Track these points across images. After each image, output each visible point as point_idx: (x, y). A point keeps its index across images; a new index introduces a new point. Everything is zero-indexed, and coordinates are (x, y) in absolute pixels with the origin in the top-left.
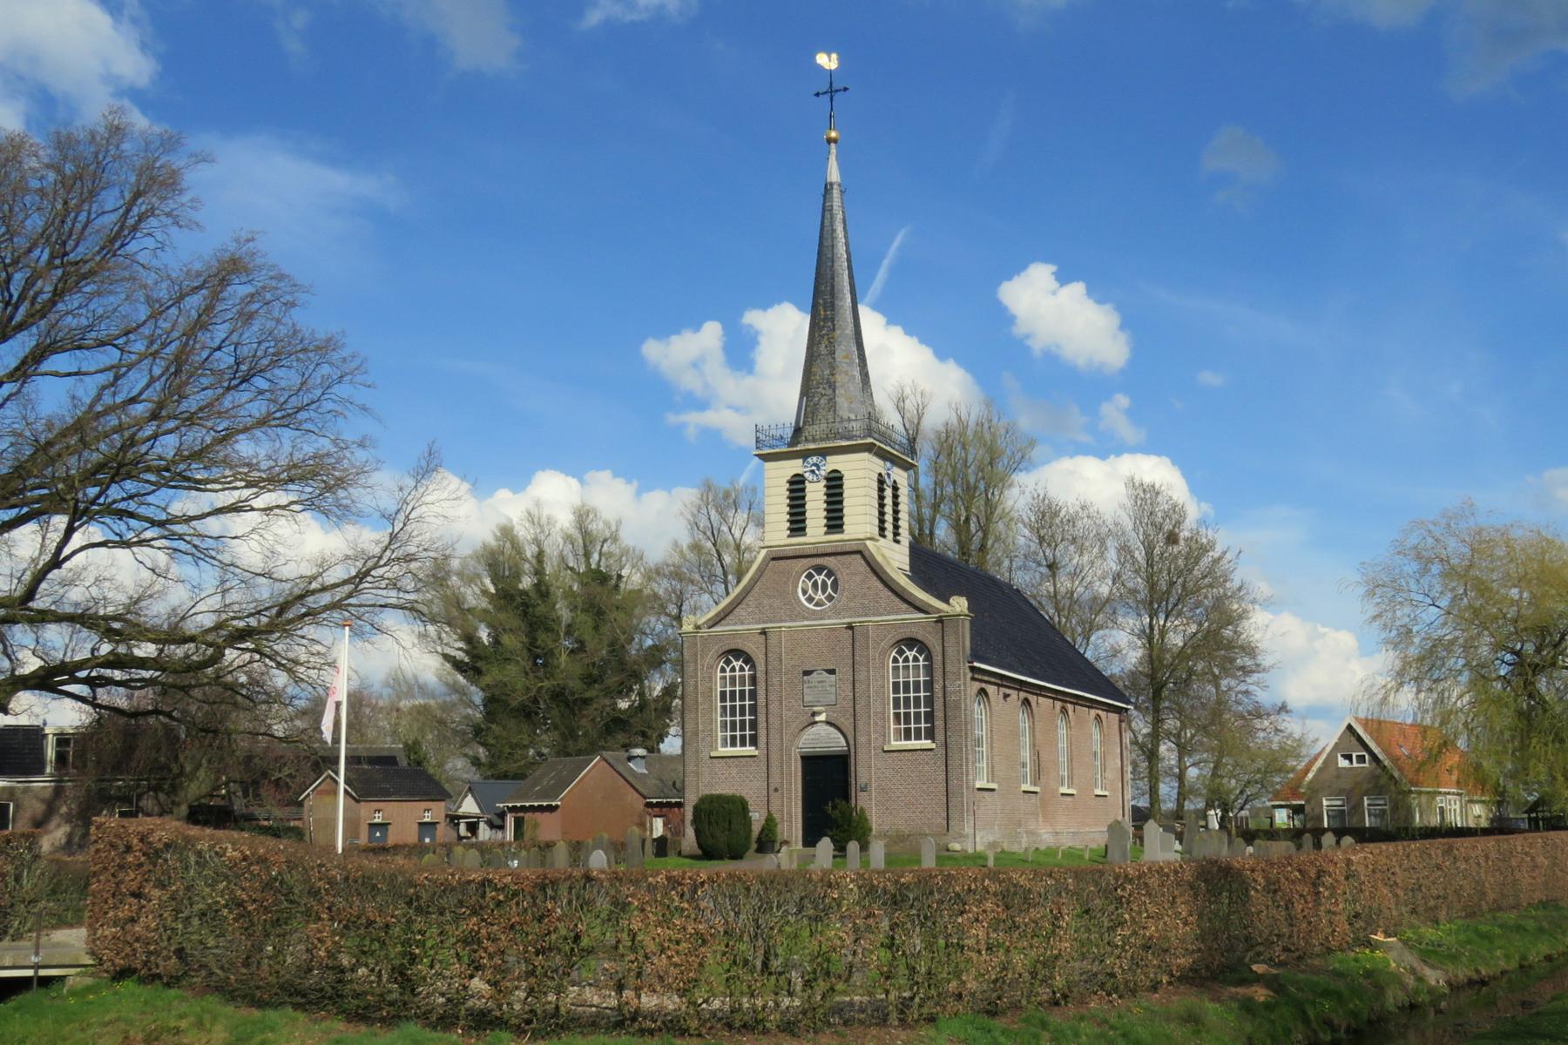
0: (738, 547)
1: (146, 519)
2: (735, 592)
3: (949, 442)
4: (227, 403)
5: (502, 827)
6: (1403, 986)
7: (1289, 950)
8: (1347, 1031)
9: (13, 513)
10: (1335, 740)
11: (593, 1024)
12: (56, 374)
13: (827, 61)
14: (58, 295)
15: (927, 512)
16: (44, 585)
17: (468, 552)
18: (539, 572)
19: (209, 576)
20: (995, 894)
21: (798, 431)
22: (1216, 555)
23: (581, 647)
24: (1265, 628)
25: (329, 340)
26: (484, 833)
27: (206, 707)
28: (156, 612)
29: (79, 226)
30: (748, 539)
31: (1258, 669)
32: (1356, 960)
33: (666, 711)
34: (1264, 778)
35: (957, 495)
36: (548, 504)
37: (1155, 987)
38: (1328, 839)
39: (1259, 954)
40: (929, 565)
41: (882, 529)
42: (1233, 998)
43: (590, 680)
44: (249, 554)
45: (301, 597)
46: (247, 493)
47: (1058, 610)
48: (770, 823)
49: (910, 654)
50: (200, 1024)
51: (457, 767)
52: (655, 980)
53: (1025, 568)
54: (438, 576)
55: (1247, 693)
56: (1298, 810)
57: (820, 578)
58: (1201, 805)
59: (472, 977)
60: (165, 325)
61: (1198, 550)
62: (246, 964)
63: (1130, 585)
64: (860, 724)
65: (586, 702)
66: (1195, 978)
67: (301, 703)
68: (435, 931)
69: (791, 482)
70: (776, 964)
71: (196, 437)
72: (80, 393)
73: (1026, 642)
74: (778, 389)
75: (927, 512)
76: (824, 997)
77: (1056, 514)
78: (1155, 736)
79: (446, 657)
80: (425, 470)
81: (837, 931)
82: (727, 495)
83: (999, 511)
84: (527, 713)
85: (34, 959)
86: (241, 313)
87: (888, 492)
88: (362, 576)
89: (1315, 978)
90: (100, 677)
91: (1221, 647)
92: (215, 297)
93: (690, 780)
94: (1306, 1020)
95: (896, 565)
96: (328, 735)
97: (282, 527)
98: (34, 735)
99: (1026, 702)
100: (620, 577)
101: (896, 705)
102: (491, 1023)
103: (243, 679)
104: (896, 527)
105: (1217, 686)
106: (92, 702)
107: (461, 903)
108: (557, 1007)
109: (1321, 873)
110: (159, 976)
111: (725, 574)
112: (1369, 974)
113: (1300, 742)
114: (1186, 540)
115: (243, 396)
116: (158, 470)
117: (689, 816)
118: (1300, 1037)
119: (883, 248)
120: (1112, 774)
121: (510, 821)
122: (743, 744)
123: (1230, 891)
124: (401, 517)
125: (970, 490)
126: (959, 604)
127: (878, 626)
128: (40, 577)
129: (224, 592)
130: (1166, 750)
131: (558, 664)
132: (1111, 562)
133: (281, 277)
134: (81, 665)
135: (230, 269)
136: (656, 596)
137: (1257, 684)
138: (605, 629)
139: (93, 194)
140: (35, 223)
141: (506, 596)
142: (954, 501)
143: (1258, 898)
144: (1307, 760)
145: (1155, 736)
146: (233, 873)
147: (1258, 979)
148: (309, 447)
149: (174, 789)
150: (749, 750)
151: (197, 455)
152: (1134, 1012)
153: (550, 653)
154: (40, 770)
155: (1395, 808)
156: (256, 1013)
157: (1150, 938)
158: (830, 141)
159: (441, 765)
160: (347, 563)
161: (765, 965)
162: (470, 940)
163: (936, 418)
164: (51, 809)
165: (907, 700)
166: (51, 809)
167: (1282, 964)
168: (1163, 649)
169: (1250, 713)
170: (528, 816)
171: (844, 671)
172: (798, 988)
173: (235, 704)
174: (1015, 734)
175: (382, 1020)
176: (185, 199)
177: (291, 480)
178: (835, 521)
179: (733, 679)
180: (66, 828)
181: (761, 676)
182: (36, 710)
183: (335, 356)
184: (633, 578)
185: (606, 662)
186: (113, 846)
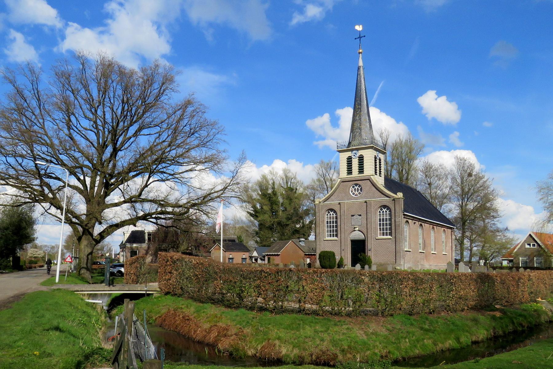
0: (331, 180)
1: (169, 174)
2: (330, 193)
3: (396, 147)
4: (188, 141)
5: (264, 260)
6: (547, 315)
7: (508, 302)
8: (528, 327)
9: (135, 173)
10: (525, 239)
11: (292, 311)
12: (144, 135)
13: (359, 28)
14: (144, 113)
15: (389, 168)
16: (143, 192)
17: (253, 181)
18: (273, 188)
19: (185, 189)
20: (412, 279)
21: (350, 143)
22: (485, 180)
23: (286, 209)
24: (502, 204)
25: (214, 122)
26: (259, 261)
27: (185, 225)
28: (172, 199)
29: (148, 93)
30: (334, 177)
31: (499, 216)
32: (531, 306)
33: (310, 228)
34: (499, 250)
35: (399, 163)
36: (276, 170)
37: (463, 310)
38: (522, 270)
39: (498, 303)
40: (390, 183)
41: (376, 172)
42: (488, 315)
43: (288, 219)
44: (196, 183)
45: (210, 194)
46: (194, 166)
47: (432, 198)
48: (341, 260)
49: (384, 210)
50: (187, 307)
51: (251, 243)
52: (310, 300)
53: (420, 184)
54: (246, 189)
55: (494, 224)
56: (511, 261)
57: (356, 188)
58: (478, 259)
59: (258, 297)
60: (171, 120)
61: (479, 178)
62: (198, 292)
63: (455, 190)
64: (369, 231)
65: (287, 225)
66: (475, 308)
67: (210, 225)
68: (248, 284)
69: (348, 159)
70: (345, 297)
71: (180, 151)
72: (151, 139)
73: (421, 207)
74: (344, 132)
75: (389, 168)
76: (359, 307)
77: (431, 168)
78: (463, 237)
79: (248, 212)
80: (242, 160)
81: (362, 288)
82: (328, 164)
83: (412, 167)
84: (271, 228)
85: (145, 289)
86: (191, 116)
87: (378, 161)
88: (225, 188)
89: (517, 311)
90: (158, 217)
91: (485, 209)
92: (184, 111)
93: (318, 246)
94: (513, 323)
95: (380, 183)
96: (217, 231)
97: (203, 175)
98: (142, 233)
99: (421, 225)
100: (296, 189)
101: (380, 225)
102: (264, 309)
103: (194, 218)
104: (380, 172)
105: (484, 222)
106: (156, 224)
107: (255, 276)
108: (282, 306)
109: (520, 278)
110: (176, 294)
111: (327, 188)
112: (535, 311)
113: (512, 240)
114: (475, 175)
115: (192, 138)
116: (171, 160)
117: (318, 257)
118: (511, 328)
119: (376, 87)
120: (449, 248)
121: (266, 258)
122: (333, 236)
123: (488, 283)
124: (235, 172)
125: (403, 161)
126: (400, 195)
127: (374, 201)
128: (142, 190)
129: (189, 193)
130: (467, 243)
131: (280, 214)
132: (449, 183)
133: (201, 105)
134: (153, 214)
135: (188, 103)
136: (307, 195)
137: (498, 221)
138: (292, 204)
139: (151, 84)
140: (138, 93)
141: (264, 195)
142: (398, 165)
143: (498, 285)
144: (513, 246)
145: (463, 237)
146: (195, 267)
147: (497, 310)
148: (210, 153)
149: (178, 247)
150: (335, 238)
151: (181, 155)
152: (456, 317)
153: (277, 211)
154: (144, 243)
155: (545, 261)
156: (201, 304)
157: (462, 295)
158: (359, 53)
159: (247, 243)
160: (220, 187)
161: (342, 297)
162: (258, 287)
163: (391, 141)
164: (147, 253)
165: (383, 224)
166: (147, 253)
167: (505, 306)
168: (466, 210)
169: (495, 230)
170: (271, 257)
171: (364, 216)
172: (351, 304)
173: (192, 224)
174: (417, 235)
175: (234, 308)
176: (175, 84)
177: (206, 162)
178: (361, 170)
179: (330, 217)
180: (151, 258)
181: (339, 217)
182: (143, 226)
183: (216, 127)
184: (300, 190)
185: (293, 214)
186: (164, 260)
